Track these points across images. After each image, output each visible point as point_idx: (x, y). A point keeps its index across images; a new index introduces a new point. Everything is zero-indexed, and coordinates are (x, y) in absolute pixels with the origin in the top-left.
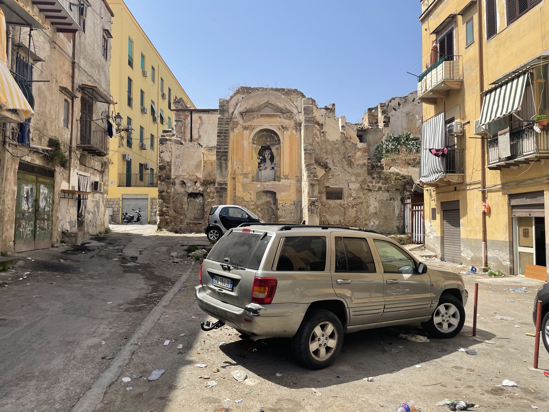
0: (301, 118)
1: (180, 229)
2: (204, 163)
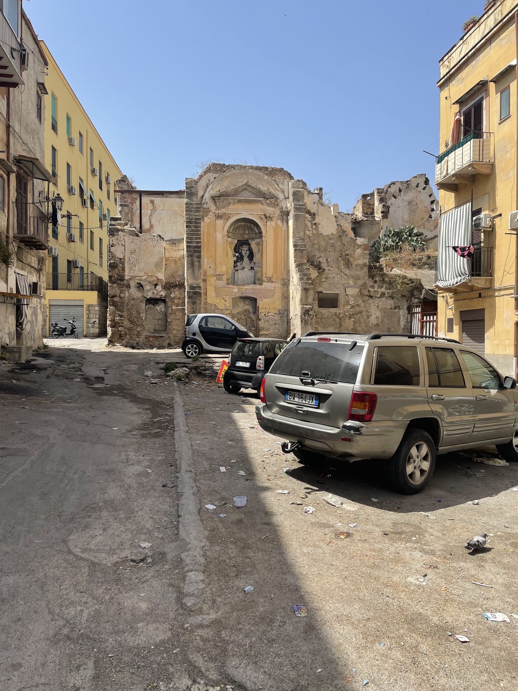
0: (289, 205)
1: (137, 343)
2: (166, 260)
